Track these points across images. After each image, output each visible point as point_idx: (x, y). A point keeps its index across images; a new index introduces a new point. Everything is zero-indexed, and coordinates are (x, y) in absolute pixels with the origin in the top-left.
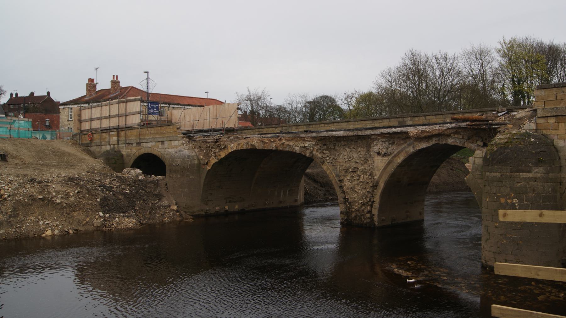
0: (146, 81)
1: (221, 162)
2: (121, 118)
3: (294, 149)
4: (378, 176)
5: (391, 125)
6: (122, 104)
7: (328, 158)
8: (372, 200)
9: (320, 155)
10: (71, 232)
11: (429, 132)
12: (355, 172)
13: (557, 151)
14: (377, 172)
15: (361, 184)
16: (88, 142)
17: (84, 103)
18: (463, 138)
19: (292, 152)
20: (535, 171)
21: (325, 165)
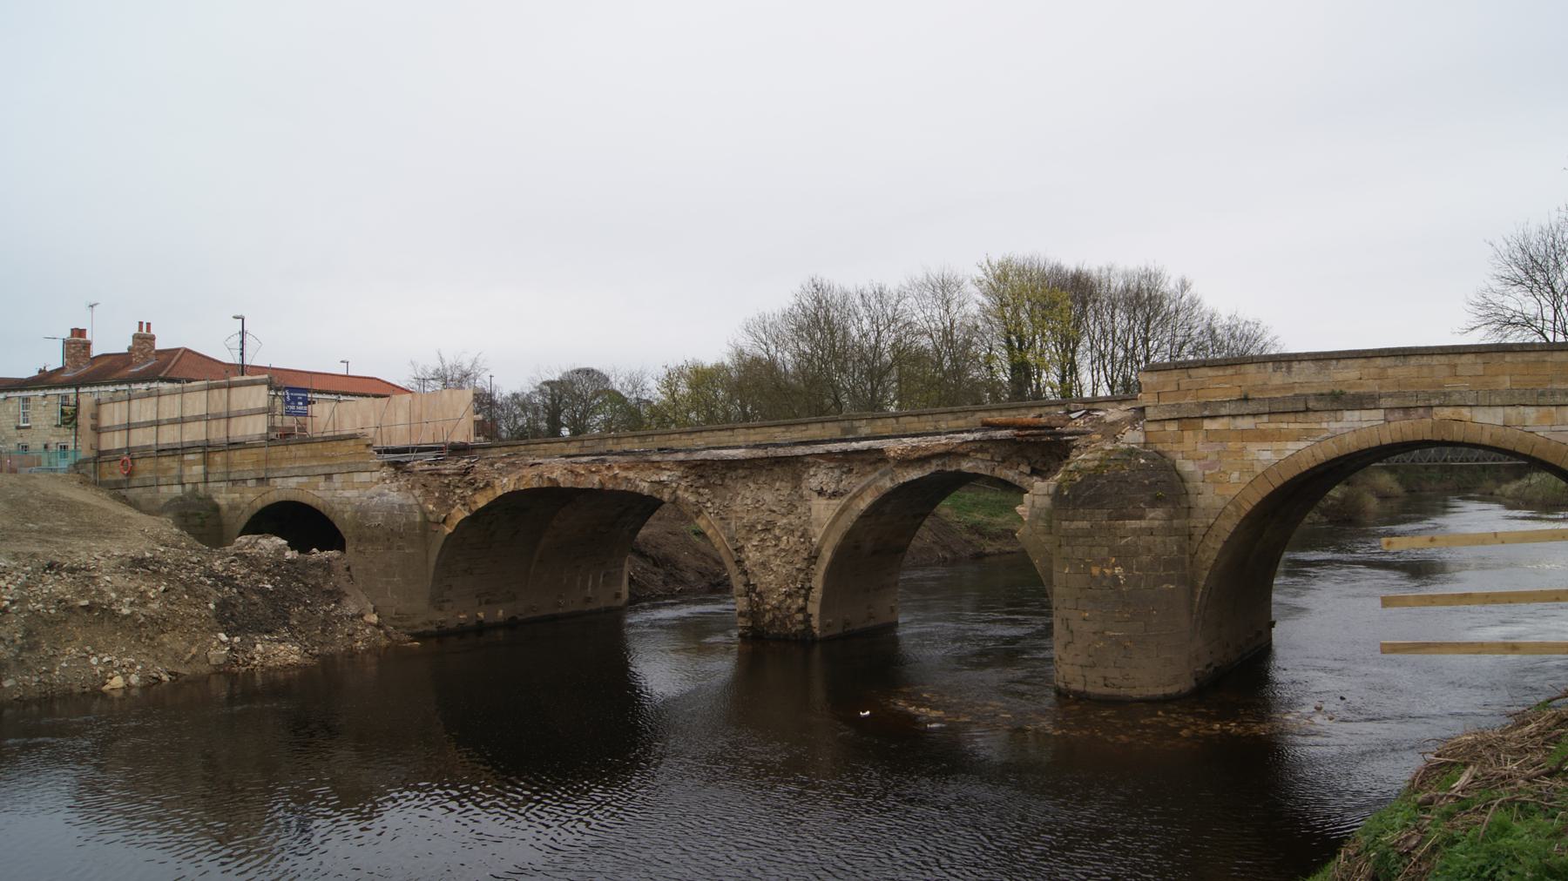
0: (239, 338)
1: (476, 517)
2: (214, 422)
3: (637, 486)
4: (820, 536)
5: (827, 435)
6: (216, 392)
7: (709, 505)
8: (807, 585)
9: (692, 499)
10: (165, 678)
11: (926, 448)
12: (769, 530)
13: (1183, 480)
14: (817, 530)
15: (783, 554)
16: (121, 477)
17: (63, 387)
18: (992, 460)
19: (633, 493)
20: (1151, 515)
21: (703, 519)
